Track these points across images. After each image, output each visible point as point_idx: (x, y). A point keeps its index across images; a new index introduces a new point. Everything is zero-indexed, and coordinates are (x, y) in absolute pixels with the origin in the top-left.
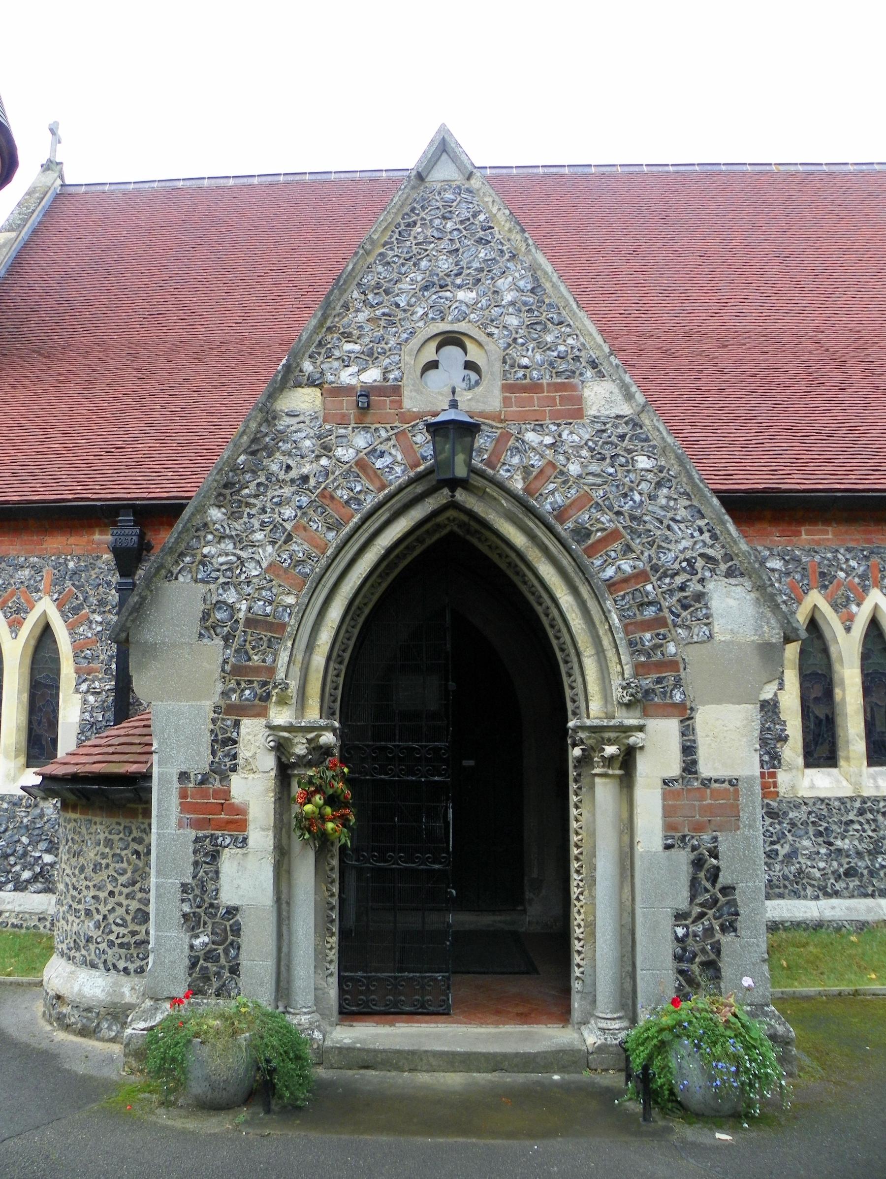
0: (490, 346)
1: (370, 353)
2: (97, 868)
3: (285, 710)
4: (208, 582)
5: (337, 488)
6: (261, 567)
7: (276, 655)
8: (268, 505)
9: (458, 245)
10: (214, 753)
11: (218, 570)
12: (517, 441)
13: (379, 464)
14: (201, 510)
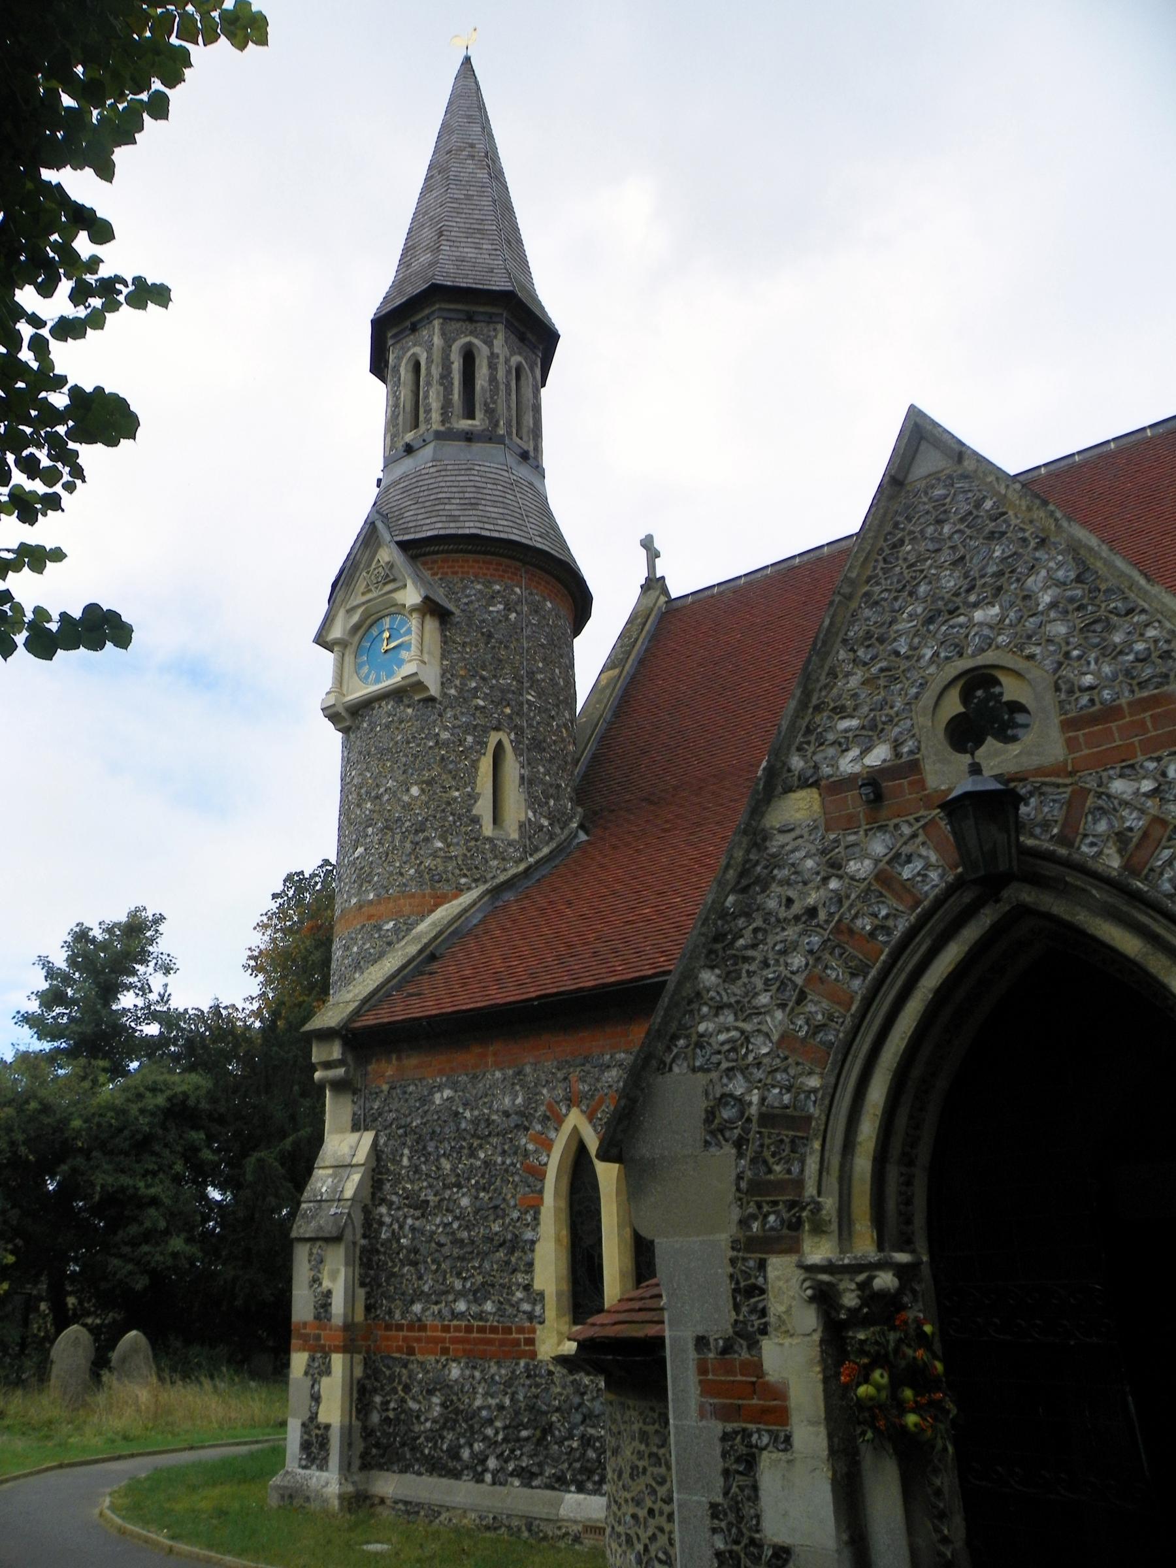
0: (1034, 673)
1: (873, 726)
2: (635, 1472)
3: (823, 1241)
4: (708, 1070)
5: (856, 916)
6: (771, 1041)
7: (803, 1162)
8: (771, 955)
9: (962, 551)
10: (737, 1307)
11: (719, 1052)
12: (1099, 797)
13: (907, 873)
14: (689, 975)
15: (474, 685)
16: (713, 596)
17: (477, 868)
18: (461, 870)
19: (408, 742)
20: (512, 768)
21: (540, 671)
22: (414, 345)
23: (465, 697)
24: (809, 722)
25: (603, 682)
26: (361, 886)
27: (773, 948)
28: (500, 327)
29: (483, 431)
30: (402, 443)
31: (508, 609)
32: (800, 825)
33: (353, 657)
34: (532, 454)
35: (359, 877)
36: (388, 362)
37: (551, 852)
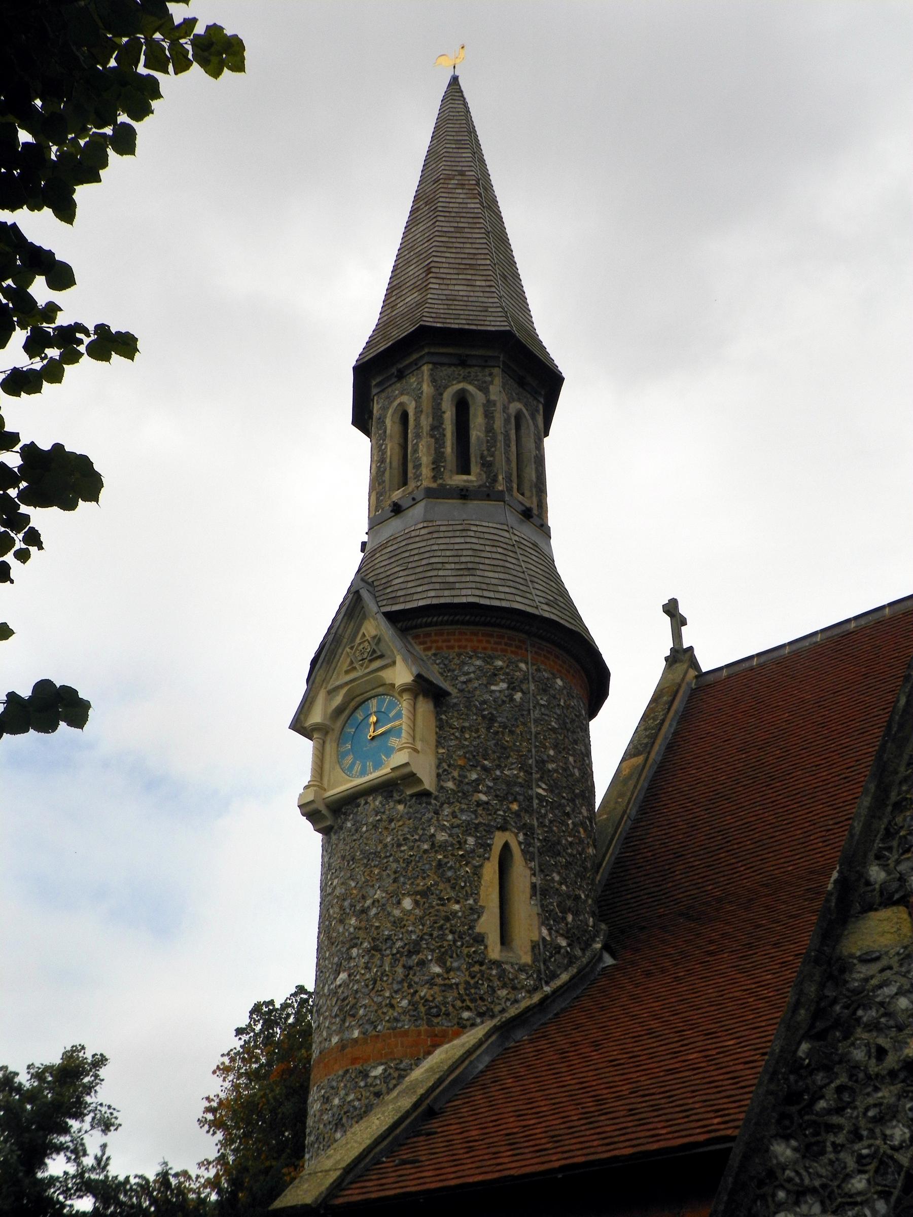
8: (862, 1122)
15: (474, 776)
16: (752, 669)
17: (482, 999)
18: (463, 1001)
19: (399, 845)
20: (522, 876)
21: (552, 760)
22: (402, 394)
23: (464, 791)
24: (890, 822)
25: (626, 772)
26: (344, 1021)
27: (865, 1114)
28: (496, 371)
29: (480, 487)
30: (389, 502)
31: (512, 687)
32: (887, 953)
33: (334, 745)
34: (535, 511)
35: (341, 1009)
36: (371, 412)
37: (571, 979)
